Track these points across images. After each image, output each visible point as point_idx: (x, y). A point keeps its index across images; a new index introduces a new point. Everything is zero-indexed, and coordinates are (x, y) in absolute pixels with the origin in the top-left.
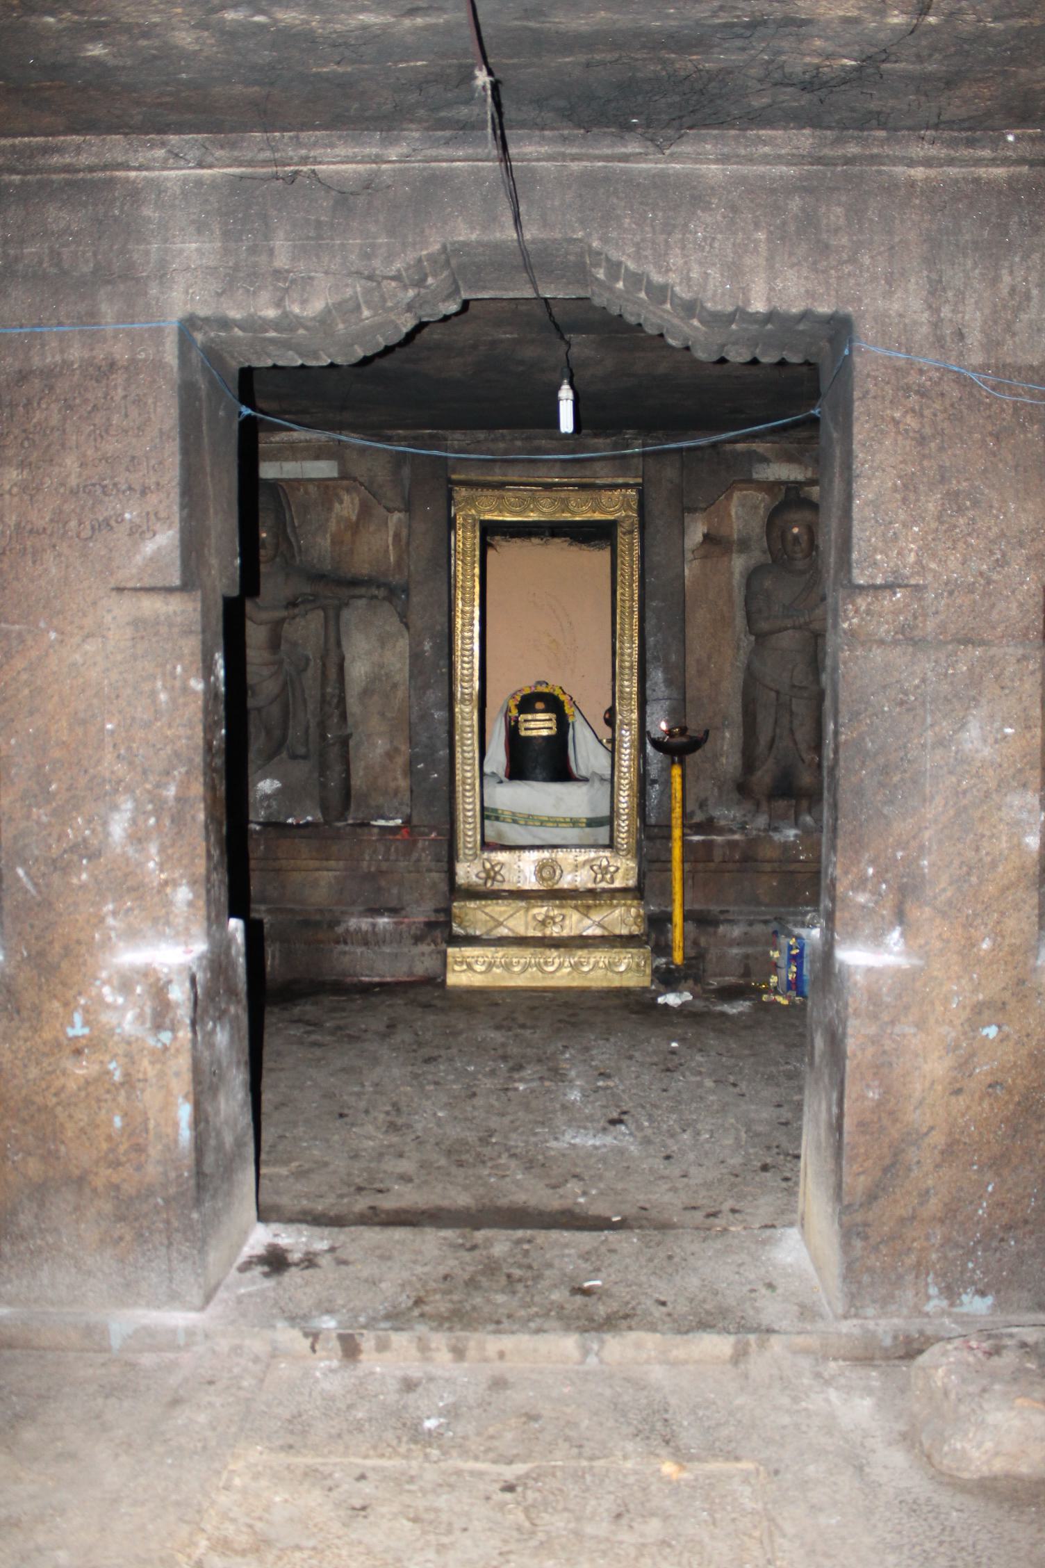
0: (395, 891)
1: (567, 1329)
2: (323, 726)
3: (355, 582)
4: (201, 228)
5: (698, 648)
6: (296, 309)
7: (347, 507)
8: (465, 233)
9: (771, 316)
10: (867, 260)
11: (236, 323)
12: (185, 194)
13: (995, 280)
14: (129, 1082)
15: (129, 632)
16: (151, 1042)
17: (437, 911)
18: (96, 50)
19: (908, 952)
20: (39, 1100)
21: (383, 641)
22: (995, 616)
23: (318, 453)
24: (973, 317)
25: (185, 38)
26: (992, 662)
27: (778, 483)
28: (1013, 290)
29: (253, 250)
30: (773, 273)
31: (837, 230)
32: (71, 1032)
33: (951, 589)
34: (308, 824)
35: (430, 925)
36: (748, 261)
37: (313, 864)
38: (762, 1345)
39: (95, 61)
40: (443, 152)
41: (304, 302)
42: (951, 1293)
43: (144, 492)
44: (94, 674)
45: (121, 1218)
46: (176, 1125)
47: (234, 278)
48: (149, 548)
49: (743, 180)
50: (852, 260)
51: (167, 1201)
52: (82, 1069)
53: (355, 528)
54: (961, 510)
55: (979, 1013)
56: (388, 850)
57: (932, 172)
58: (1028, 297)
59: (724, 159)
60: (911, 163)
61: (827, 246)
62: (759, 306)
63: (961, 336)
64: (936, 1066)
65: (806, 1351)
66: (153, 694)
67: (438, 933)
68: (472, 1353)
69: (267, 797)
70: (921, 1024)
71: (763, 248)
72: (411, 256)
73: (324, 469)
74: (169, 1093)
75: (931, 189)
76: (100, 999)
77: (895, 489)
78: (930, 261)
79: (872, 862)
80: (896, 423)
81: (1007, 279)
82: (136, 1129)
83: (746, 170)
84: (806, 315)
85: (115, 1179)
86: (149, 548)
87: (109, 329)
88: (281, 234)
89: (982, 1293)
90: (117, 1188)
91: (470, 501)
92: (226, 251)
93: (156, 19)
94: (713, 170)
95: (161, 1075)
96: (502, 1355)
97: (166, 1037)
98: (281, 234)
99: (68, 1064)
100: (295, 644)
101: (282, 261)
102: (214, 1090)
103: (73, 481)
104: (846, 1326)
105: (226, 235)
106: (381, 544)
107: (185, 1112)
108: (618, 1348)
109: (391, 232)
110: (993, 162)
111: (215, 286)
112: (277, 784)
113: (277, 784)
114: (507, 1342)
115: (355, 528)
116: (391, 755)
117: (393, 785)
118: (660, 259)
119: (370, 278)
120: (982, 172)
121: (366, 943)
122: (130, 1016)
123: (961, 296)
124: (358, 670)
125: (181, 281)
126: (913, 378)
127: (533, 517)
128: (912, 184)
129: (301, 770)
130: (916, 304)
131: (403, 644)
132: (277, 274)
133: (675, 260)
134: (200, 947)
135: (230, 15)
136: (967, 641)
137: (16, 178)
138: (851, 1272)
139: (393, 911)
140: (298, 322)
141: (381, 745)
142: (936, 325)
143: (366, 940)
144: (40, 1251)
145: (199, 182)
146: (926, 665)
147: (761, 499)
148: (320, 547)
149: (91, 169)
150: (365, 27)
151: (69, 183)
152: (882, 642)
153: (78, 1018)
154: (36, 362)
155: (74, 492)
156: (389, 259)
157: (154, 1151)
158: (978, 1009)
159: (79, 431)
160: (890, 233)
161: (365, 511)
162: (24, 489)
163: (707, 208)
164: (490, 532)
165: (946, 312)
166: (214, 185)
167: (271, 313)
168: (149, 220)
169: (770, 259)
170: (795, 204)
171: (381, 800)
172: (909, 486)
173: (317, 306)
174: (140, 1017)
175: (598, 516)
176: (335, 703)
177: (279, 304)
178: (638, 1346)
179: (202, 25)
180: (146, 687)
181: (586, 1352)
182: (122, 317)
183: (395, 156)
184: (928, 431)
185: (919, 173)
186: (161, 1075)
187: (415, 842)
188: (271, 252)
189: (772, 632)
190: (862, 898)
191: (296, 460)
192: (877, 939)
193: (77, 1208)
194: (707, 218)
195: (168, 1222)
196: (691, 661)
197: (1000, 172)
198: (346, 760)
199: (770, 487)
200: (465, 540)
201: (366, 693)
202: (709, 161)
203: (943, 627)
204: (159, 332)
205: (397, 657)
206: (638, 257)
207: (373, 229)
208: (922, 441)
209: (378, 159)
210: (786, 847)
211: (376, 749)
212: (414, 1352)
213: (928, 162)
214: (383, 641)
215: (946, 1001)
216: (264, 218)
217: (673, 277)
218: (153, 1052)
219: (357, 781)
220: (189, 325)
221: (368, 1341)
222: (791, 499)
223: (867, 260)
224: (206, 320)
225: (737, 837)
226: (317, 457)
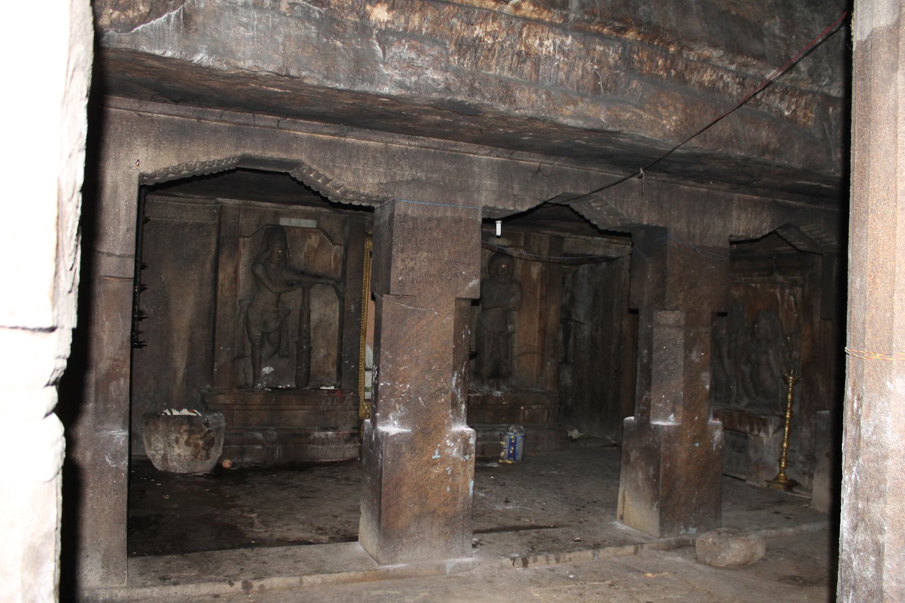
0: (333, 420)
1: (589, 549)
3: (317, 276)
7: (314, 241)
16: (462, 459)
17: (354, 428)
19: (676, 421)
21: (326, 304)
23: (308, 216)
32: (433, 457)
34: (288, 389)
35: (352, 435)
37: (297, 407)
38: (642, 548)
42: (686, 528)
45: (446, 525)
48: (471, 284)
51: (464, 517)
52: (437, 470)
53: (316, 251)
55: (694, 439)
56: (333, 401)
62: (645, 223)
64: (683, 456)
65: (654, 548)
67: (356, 438)
68: (561, 560)
69: (267, 375)
70: (681, 443)
73: (310, 223)
74: (467, 478)
76: (446, 443)
79: (664, 394)
82: (455, 491)
85: (446, 511)
86: (471, 284)
89: (694, 527)
90: (446, 514)
95: (465, 470)
96: (570, 559)
97: (467, 457)
101: (515, 192)
104: (662, 540)
106: (329, 258)
108: (603, 553)
112: (272, 369)
113: (272, 369)
114: (572, 555)
115: (316, 251)
116: (326, 357)
117: (327, 370)
121: (323, 443)
122: (455, 450)
125: (484, 194)
138: (662, 523)
139: (334, 429)
141: (323, 352)
142: (689, 232)
143: (323, 442)
144: (417, 540)
148: (299, 259)
153: (437, 452)
154: (435, 215)
157: (460, 499)
161: (322, 244)
166: (497, 162)
171: (322, 377)
174: (459, 450)
177: (514, 206)
178: (608, 551)
181: (594, 555)
186: (465, 470)
187: (345, 397)
188: (513, 188)
190: (660, 405)
191: (296, 218)
192: (665, 418)
193: (432, 523)
195: (463, 525)
198: (309, 357)
204: (476, 210)
210: (498, 398)
211: (323, 353)
212: (544, 561)
214: (326, 304)
217: (624, 212)
218: (463, 463)
219: (313, 369)
220: (485, 208)
221: (531, 560)
225: (478, 394)
226: (307, 218)
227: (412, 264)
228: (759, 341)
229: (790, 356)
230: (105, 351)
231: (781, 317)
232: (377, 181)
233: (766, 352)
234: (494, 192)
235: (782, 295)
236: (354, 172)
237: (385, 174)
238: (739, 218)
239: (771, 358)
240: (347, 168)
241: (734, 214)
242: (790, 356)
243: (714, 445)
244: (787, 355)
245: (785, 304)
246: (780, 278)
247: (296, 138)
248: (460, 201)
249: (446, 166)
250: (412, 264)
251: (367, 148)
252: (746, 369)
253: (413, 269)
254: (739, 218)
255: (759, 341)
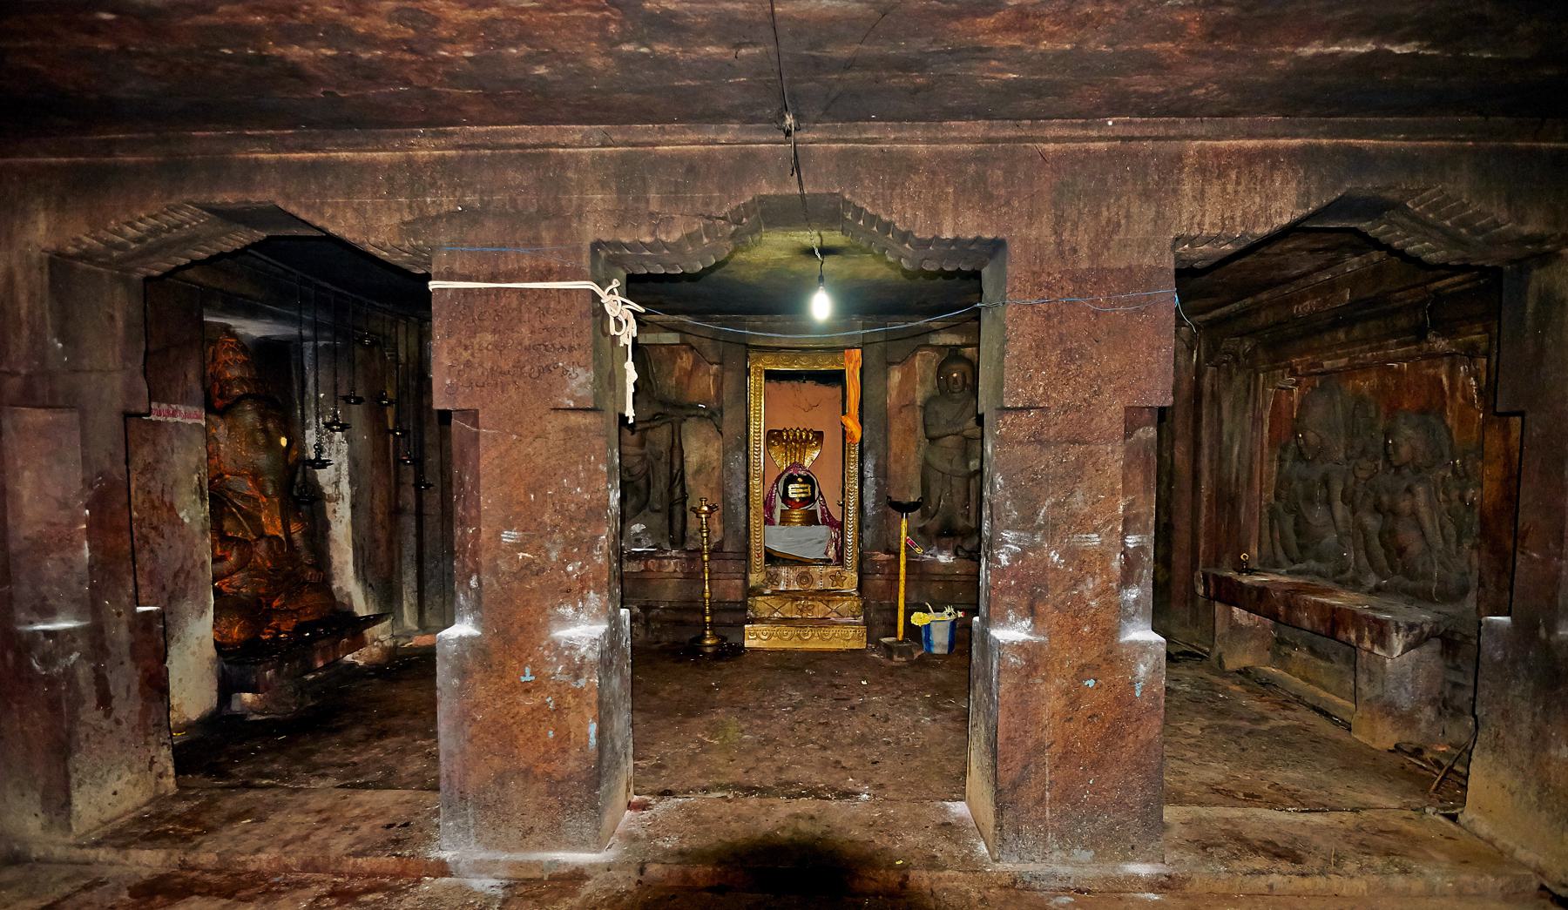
2: (671, 491)
4: (604, 185)
5: (895, 445)
6: (663, 238)
7: (686, 361)
8: (767, 190)
9: (956, 240)
10: (1016, 204)
11: (625, 246)
12: (593, 163)
13: (1097, 215)
14: (558, 709)
15: (562, 435)
18: (541, 70)
20: (502, 721)
22: (1093, 426)
24: (1083, 239)
25: (597, 62)
26: (1091, 454)
27: (945, 346)
28: (1109, 220)
29: (636, 200)
30: (957, 215)
31: (998, 185)
33: (1066, 408)
36: (941, 206)
39: (540, 77)
40: (754, 137)
41: (668, 233)
43: (571, 349)
44: (540, 460)
46: (588, 735)
47: (623, 217)
49: (939, 154)
50: (1008, 203)
52: (529, 702)
53: (690, 374)
54: (1072, 361)
57: (1058, 146)
58: (1119, 225)
59: (929, 141)
60: (1045, 141)
61: (992, 195)
62: (948, 235)
63: (1075, 251)
66: (577, 473)
71: (951, 197)
72: (734, 204)
73: (672, 338)
75: (1059, 157)
77: (1031, 348)
78: (1055, 204)
80: (1033, 306)
81: (1105, 213)
83: (940, 147)
84: (977, 240)
87: (548, 248)
88: (653, 189)
89: (1085, 848)
90: (549, 775)
91: (758, 359)
92: (619, 199)
93: (579, 50)
94: (921, 148)
98: (653, 189)
99: (521, 698)
100: (654, 444)
101: (654, 207)
102: (609, 713)
103: (526, 342)
105: (619, 191)
107: (593, 728)
109: (722, 189)
110: (1100, 139)
111: (614, 222)
115: (690, 374)
118: (888, 207)
119: (709, 218)
120: (1091, 145)
123: (1075, 225)
124: (693, 458)
126: (1044, 278)
127: (796, 368)
128: (1043, 155)
129: (657, 519)
130: (1047, 231)
131: (717, 444)
132: (652, 215)
133: (897, 206)
134: (601, 628)
135: (626, 48)
136: (1074, 442)
137: (488, 152)
140: (665, 245)
142: (1060, 244)
145: (602, 156)
146: (1049, 456)
147: (934, 357)
149: (535, 146)
150: (709, 55)
151: (522, 156)
152: (1020, 443)
153: (528, 670)
155: (527, 349)
156: (720, 206)
157: (574, 752)
158: (1082, 668)
159: (530, 311)
160: (1031, 186)
161: (696, 365)
162: (496, 347)
163: (917, 172)
164: (770, 375)
165: (1066, 236)
166: (611, 158)
167: (648, 239)
168: (571, 180)
169: (956, 206)
170: (972, 169)
172: (1039, 345)
173: (676, 236)
175: (835, 367)
176: (677, 478)
177: (653, 234)
179: (608, 54)
180: (573, 469)
182: (557, 240)
183: (726, 138)
184: (1052, 311)
185: (1050, 147)
188: (647, 201)
189: (940, 437)
194: (916, 178)
196: (891, 454)
197: (1102, 145)
199: (939, 348)
200: (755, 382)
201: (698, 471)
202: (917, 142)
203: (1059, 433)
205: (713, 452)
206: (873, 204)
207: (710, 186)
208: (1048, 317)
209: (715, 142)
213: (1056, 140)
215: (1062, 662)
216: (644, 180)
222: (952, 355)
223: (1016, 204)
224: (607, 244)
227: (466, 355)
228: (1398, 469)
229: (1462, 498)
230: (29, 513)
231: (1449, 422)
232: (396, 219)
233: (1409, 490)
234: (612, 212)
235: (1452, 377)
236: (359, 211)
237: (410, 207)
238: (1200, 196)
239: (1421, 498)
240: (345, 205)
241: (1187, 188)
242: (1462, 498)
243: (1138, 687)
244: (1455, 494)
245: (1458, 394)
246: (1441, 344)
247: (259, 165)
248: (547, 236)
249: (513, 176)
250: (466, 355)
251: (373, 166)
252: (1372, 522)
253: (468, 364)
254: (1200, 196)
255: (1398, 469)
